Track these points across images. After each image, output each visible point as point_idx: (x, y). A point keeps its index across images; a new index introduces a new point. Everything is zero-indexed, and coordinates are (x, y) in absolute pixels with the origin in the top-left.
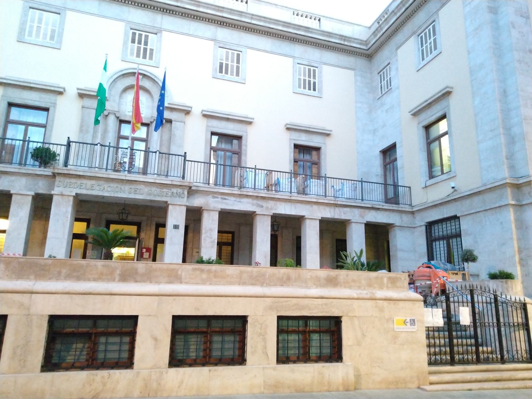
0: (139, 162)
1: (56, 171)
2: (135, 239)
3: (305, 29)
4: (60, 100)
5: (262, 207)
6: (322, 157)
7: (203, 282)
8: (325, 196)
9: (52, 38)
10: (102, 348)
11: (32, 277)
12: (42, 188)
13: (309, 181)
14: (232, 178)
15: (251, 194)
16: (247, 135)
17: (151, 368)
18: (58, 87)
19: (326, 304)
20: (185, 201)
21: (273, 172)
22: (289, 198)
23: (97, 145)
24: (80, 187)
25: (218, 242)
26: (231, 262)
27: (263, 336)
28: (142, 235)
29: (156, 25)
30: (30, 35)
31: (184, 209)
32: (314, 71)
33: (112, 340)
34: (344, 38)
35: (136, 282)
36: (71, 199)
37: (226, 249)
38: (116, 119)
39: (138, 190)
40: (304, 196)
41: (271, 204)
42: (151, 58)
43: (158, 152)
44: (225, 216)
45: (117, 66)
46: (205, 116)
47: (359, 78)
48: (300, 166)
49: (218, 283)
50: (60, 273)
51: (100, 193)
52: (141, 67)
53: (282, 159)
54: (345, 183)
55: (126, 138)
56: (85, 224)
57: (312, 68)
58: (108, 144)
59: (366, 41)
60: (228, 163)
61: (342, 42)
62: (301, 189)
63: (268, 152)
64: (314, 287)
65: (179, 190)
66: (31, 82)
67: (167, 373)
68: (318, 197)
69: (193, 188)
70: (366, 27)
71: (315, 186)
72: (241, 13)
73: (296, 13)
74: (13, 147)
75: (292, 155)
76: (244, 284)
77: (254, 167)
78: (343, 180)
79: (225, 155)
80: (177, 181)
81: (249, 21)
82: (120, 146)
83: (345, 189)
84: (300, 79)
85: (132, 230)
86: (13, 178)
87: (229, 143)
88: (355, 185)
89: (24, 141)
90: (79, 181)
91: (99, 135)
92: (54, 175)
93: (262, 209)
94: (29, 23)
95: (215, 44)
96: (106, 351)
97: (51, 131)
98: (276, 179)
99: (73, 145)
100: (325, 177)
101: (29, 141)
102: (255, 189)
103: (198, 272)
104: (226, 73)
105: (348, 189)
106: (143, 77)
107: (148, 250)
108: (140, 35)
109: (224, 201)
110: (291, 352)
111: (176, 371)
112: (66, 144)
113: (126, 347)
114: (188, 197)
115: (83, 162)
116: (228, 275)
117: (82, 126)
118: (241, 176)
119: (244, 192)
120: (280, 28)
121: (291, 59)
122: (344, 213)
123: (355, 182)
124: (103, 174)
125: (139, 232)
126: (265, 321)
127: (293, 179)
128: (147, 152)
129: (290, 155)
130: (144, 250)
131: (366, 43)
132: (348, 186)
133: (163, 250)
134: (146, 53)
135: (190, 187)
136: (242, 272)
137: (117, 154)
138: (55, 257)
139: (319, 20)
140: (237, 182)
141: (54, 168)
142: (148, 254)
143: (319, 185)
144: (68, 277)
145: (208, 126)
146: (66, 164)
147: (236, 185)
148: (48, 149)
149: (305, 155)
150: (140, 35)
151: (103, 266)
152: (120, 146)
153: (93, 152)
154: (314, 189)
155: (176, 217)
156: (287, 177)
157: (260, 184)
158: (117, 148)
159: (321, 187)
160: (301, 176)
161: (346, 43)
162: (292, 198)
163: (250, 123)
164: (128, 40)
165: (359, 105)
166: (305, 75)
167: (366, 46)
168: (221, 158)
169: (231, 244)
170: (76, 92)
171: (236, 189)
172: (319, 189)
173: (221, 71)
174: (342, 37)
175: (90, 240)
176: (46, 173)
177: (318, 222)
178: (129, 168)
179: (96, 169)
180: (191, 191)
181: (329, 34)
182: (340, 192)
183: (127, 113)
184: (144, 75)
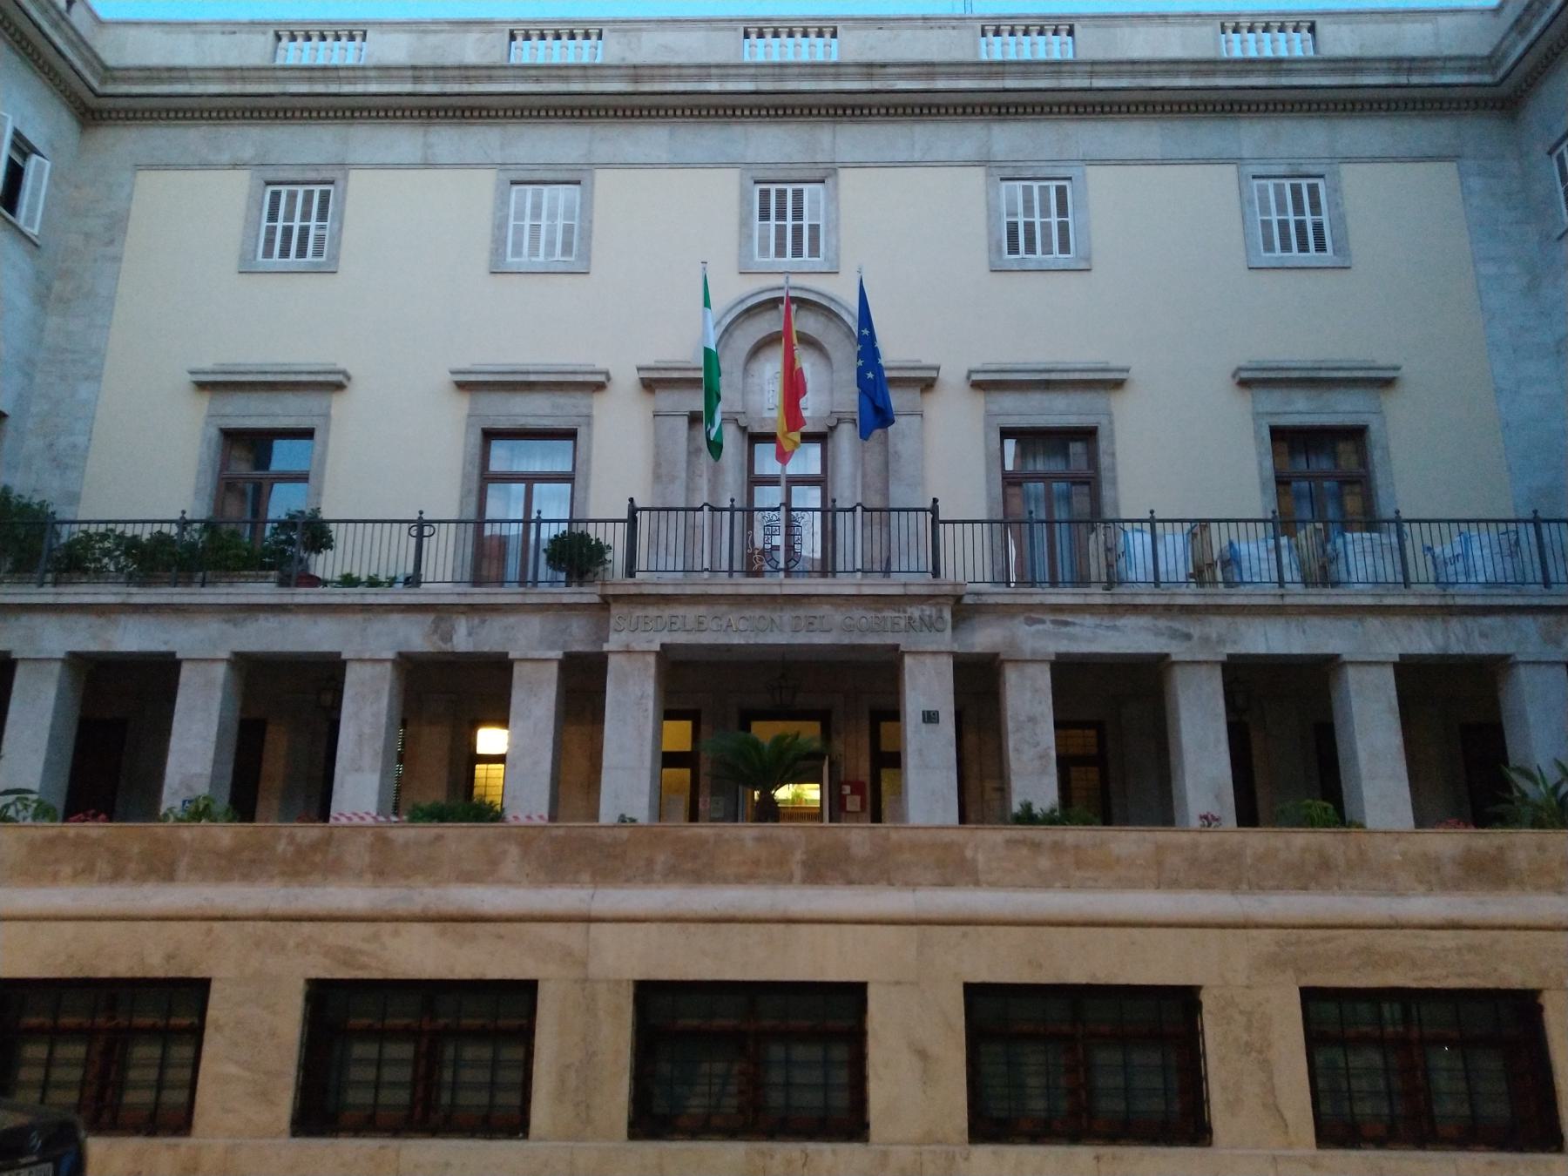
0: (810, 546)
1: (610, 591)
2: (817, 756)
3: (1266, 67)
4: (599, 403)
5: (1188, 637)
6: (1376, 455)
7: (1044, 882)
8: (1407, 583)
9: (567, 248)
10: (776, 1076)
11: (585, 877)
12: (578, 637)
13: (1339, 541)
14: (1079, 554)
15: (1146, 600)
16: (1111, 423)
17: (920, 1143)
18: (592, 373)
19: (1471, 948)
20: (946, 640)
21: (1214, 526)
22: (1278, 601)
23: (701, 509)
24: (671, 627)
25: (1058, 756)
26: (1106, 816)
27: (1260, 1052)
28: (838, 745)
29: (819, 158)
30: (517, 252)
31: (947, 665)
32: (1313, 190)
33: (800, 1052)
34: (1406, 65)
35: (850, 882)
36: (652, 659)
37: (1086, 777)
38: (739, 435)
39: (816, 622)
40: (1329, 590)
41: (1216, 626)
42: (814, 251)
43: (859, 509)
44: (1073, 677)
45: (732, 290)
46: (978, 386)
47: (1476, 183)
48: (1298, 496)
49: (1090, 883)
50: (650, 862)
51: (722, 639)
52: (795, 281)
53: (1238, 481)
54: (1474, 533)
55: (772, 481)
56: (686, 726)
57: (1304, 183)
58: (728, 504)
59: (1489, 58)
60: (1060, 513)
61: (1403, 80)
62: (1315, 566)
63: (1184, 464)
64: (1422, 889)
65: (928, 610)
66: (531, 369)
67: (966, 1159)
68: (1379, 590)
69: (968, 600)
70: (1482, 12)
71: (1361, 555)
72: (1055, 67)
73: (1230, 25)
74: (503, 541)
75: (1268, 462)
76: (1174, 884)
77: (1148, 516)
78: (1463, 526)
79: (1048, 491)
80: (920, 584)
81: (1085, 83)
82: (757, 505)
83: (1477, 553)
84: (1266, 225)
85: (809, 732)
86: (512, 619)
87: (1056, 457)
88: (1513, 537)
89: (526, 522)
90: (667, 612)
91: (704, 484)
92: (606, 602)
93: (1187, 644)
94: (511, 223)
95: (988, 175)
96: (788, 1084)
97: (586, 488)
98: (1225, 543)
99: (643, 517)
100: (1398, 521)
101: (539, 521)
102: (1157, 583)
103: (1025, 851)
104: (1031, 249)
105: (1486, 551)
106: (799, 307)
107: (858, 788)
108: (781, 194)
109: (1064, 630)
110: (1365, 1109)
111: (994, 1153)
112: (625, 516)
113: (842, 1076)
114: (954, 628)
115: (671, 560)
116: (1118, 860)
117: (657, 465)
118: (1108, 550)
119: (1123, 595)
120: (1185, 82)
121: (1231, 170)
122: (1483, 635)
123: (1512, 526)
124: (723, 585)
125: (826, 733)
126: (1260, 1004)
127: (1284, 541)
128: (828, 511)
129: (1260, 464)
130: (847, 789)
131: (1490, 61)
132: (1485, 540)
133: (900, 791)
134: (801, 241)
135: (958, 598)
136: (1160, 848)
137: (750, 526)
138: (633, 821)
139: (1312, 29)
140: (1096, 568)
141: (604, 585)
142: (858, 798)
143: (1378, 549)
144: (673, 874)
145: (989, 415)
146: (631, 570)
147: (1530, 579)
148: (584, 537)
149: (1313, 460)
150: (781, 194)
151: (758, 840)
152: (757, 505)
153: (691, 530)
154: (1360, 565)
155: (927, 688)
156: (1261, 534)
157: (1171, 567)
158: (750, 510)
159: (1388, 556)
160: (1310, 527)
161: (1415, 79)
162: (1288, 601)
163: (1118, 384)
164: (751, 212)
165: (1491, 269)
166: (1281, 209)
167: (1493, 73)
168: (1037, 500)
169: (1099, 760)
170: (635, 376)
171: (1094, 589)
172: (1379, 563)
173: (1013, 249)
174: (1399, 63)
175: (705, 767)
176: (585, 599)
177: (1389, 674)
178: (786, 563)
179: (706, 575)
180: (964, 610)
181: (1354, 64)
182: (1460, 566)
183: (767, 414)
184: (803, 303)
